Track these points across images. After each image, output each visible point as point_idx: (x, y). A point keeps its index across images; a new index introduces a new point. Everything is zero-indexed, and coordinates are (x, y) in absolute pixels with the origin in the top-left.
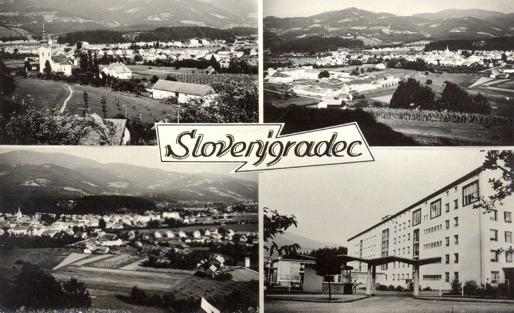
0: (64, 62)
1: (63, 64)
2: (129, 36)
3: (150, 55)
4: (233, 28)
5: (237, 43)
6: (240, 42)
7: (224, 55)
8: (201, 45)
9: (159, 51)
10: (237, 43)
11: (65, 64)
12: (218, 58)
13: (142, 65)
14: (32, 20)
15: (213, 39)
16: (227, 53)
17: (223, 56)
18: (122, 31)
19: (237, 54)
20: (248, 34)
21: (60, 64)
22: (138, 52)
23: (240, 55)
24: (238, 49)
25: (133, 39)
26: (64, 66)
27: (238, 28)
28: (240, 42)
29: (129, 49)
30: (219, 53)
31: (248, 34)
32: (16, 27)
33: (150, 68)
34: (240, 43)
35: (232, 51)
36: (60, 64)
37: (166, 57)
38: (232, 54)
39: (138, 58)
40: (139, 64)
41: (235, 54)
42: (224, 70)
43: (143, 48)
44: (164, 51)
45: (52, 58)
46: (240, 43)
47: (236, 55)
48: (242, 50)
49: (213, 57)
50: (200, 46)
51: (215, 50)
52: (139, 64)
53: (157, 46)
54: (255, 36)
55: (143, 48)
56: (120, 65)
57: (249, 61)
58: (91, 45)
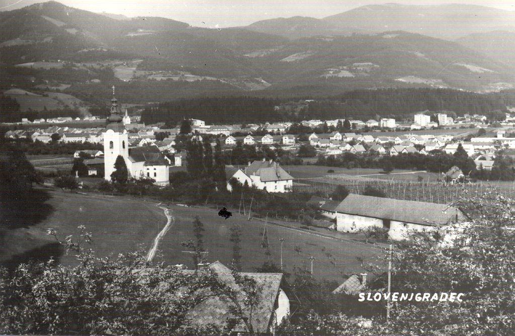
0: (154, 160)
1: (152, 164)
4: (502, 92)
5: (510, 121)
7: (483, 144)
8: (436, 125)
9: (350, 137)
10: (510, 121)
11: (157, 164)
13: (316, 164)
16: (490, 140)
17: (480, 147)
19: (509, 143)
22: (306, 139)
26: (154, 167)
30: (473, 140)
32: (58, 91)
33: (331, 172)
36: (146, 165)
37: (364, 150)
38: (499, 142)
40: (308, 164)
41: (505, 143)
43: (317, 131)
44: (360, 138)
47: (507, 145)
49: (460, 148)
50: (433, 128)
52: (308, 164)
53: (344, 129)
55: (317, 131)
56: (269, 166)
58: (209, 127)
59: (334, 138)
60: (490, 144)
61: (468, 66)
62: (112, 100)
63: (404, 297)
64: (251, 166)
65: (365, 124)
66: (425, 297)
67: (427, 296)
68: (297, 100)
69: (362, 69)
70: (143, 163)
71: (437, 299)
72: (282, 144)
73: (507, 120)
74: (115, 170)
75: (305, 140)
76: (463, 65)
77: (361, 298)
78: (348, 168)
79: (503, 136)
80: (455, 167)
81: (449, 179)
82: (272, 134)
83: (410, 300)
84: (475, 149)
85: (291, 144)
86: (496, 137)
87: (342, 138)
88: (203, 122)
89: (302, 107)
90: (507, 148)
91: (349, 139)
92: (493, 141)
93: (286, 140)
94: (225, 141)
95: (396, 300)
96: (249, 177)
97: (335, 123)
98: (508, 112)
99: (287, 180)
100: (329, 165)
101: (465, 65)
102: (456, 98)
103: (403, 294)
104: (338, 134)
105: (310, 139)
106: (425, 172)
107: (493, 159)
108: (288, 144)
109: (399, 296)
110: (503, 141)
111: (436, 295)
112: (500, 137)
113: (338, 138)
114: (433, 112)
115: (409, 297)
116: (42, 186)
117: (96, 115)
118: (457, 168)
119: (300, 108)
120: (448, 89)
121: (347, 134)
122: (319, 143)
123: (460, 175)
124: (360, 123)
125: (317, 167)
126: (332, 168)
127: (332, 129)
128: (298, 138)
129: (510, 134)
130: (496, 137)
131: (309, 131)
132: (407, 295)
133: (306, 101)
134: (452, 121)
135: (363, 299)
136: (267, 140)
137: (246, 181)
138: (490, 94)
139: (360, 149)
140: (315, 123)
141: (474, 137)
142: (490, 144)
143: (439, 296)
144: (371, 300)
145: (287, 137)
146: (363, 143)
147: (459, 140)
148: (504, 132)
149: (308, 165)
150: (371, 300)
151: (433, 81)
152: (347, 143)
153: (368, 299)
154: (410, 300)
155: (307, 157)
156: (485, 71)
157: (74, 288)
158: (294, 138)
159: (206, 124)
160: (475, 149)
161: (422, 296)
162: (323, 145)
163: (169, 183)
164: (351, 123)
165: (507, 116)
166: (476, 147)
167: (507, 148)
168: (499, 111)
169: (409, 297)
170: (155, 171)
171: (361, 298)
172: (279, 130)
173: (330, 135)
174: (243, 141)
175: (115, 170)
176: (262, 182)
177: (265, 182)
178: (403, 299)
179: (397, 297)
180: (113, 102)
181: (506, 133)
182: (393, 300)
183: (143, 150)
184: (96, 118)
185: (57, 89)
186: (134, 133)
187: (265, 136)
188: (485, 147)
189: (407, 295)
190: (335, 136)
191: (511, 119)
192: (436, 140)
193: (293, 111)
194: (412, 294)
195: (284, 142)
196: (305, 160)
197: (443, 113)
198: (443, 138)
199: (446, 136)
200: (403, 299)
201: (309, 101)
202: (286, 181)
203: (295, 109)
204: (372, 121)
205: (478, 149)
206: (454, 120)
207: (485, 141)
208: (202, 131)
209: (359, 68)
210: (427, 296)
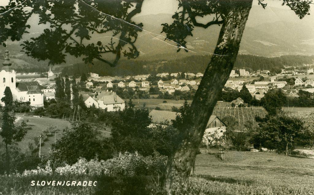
0: (33, 90)
1: (32, 92)
2: (151, 66)
3: (170, 87)
4: (282, 57)
5: (283, 73)
6: (287, 72)
7: (261, 85)
8: (238, 75)
9: (182, 82)
10: (283, 73)
11: (35, 92)
12: (252, 89)
13: (157, 98)
14: (147, 93)
15: (255, 70)
16: (266, 83)
17: (260, 87)
18: (144, 61)
19: (278, 85)
20: (300, 63)
21: (28, 93)
22: (156, 84)
23: (281, 85)
24: (280, 78)
25: (115, 48)
26: (34, 94)
27: (288, 57)
28: (287, 72)
29: (146, 80)
30: (256, 83)
31: (300, 63)
32: (14, 58)
33: (165, 102)
34: (286, 73)
35: (273, 81)
36: (28, 93)
37: (189, 89)
38: (272, 84)
39: (153, 91)
40: (153, 98)
41: (276, 84)
42: (255, 103)
43: (164, 79)
44: (188, 82)
45: (17, 85)
46: (286, 73)
47: (276, 86)
48: (285, 79)
49: (244, 88)
50: (236, 77)
51: (252, 80)
52: (153, 98)
53: (182, 77)
54: (308, 65)
55: (164, 79)
56: (110, 94)
57: (291, 92)
58: (100, 77)
59: (173, 83)
60: (266, 85)
61: (262, 42)
62: (6, 51)
63: (59, 183)
64: (100, 94)
65: (195, 75)
66: (73, 183)
67: (74, 183)
68: (157, 62)
69: (199, 44)
70: (27, 92)
71: (80, 185)
72: (141, 87)
73: (282, 73)
74: (4, 96)
75: (155, 84)
76: (259, 41)
77: (34, 182)
78: (176, 100)
79: (275, 81)
80: (239, 98)
81: (233, 105)
82: (136, 81)
83: (63, 185)
84: (256, 89)
85: (146, 87)
86: (270, 81)
87: (178, 83)
88: (98, 75)
89: (160, 66)
90: (276, 88)
91: (182, 84)
92: (268, 84)
93: (144, 84)
94: (106, 85)
95: (91, 185)
96: (97, 101)
97: (176, 75)
98: (284, 68)
99: (121, 103)
100: (165, 98)
101: (261, 42)
102: (253, 60)
103: (58, 182)
104: (176, 80)
105: (158, 84)
106: (222, 101)
107: (264, 93)
108: (145, 87)
109: (56, 183)
110: (274, 83)
111: (80, 182)
112: (273, 81)
113: (176, 83)
114: (237, 68)
115: (62, 183)
116: (33, 117)
117: (36, 72)
118: (240, 99)
119: (158, 67)
120: (248, 55)
121: (181, 81)
122: (163, 86)
123: (240, 103)
124: (192, 75)
125: (157, 99)
126: (166, 100)
127: (174, 77)
128: (151, 83)
129: (279, 79)
130: (270, 81)
131: (159, 78)
132: (61, 182)
133: (163, 62)
134: (249, 73)
135: (34, 184)
136: (132, 84)
137: (93, 104)
138: (275, 58)
139: (187, 89)
140: (164, 75)
141: (257, 81)
142: (266, 85)
143: (82, 183)
144: (40, 185)
145: (144, 83)
146: (189, 85)
147: (247, 84)
148: (275, 78)
149: (153, 98)
150: (40, 185)
151: (241, 51)
152: (180, 85)
153: (38, 184)
154: (63, 185)
155: (153, 94)
156: (272, 45)
157: (76, 174)
158: (149, 83)
159: (99, 76)
160: (256, 89)
161: (71, 183)
162: (166, 87)
163: (43, 105)
164: (186, 74)
165: (282, 71)
166: (257, 87)
167: (276, 88)
168: (277, 68)
169: (62, 183)
170: (30, 98)
171: (34, 182)
172: (142, 79)
173: (171, 81)
174: (117, 85)
175: (4, 96)
176: (104, 104)
177: (107, 104)
178: (59, 184)
179: (55, 183)
180: (6, 52)
181: (276, 79)
182: (53, 185)
183: (27, 84)
184: (36, 74)
185: (14, 56)
186: (53, 81)
187: (131, 82)
188: (263, 87)
189: (61, 182)
190: (174, 82)
191: (285, 72)
192: (233, 83)
193: (154, 69)
194: (64, 182)
195: (142, 86)
196: (151, 96)
197: (243, 69)
198: (238, 82)
199: (240, 81)
200: (59, 184)
201: (164, 62)
202: (121, 104)
203: (156, 67)
204: (199, 73)
205: (258, 88)
206: (250, 73)
207: (263, 84)
208: (95, 80)
209: (197, 43)
210: (74, 183)
